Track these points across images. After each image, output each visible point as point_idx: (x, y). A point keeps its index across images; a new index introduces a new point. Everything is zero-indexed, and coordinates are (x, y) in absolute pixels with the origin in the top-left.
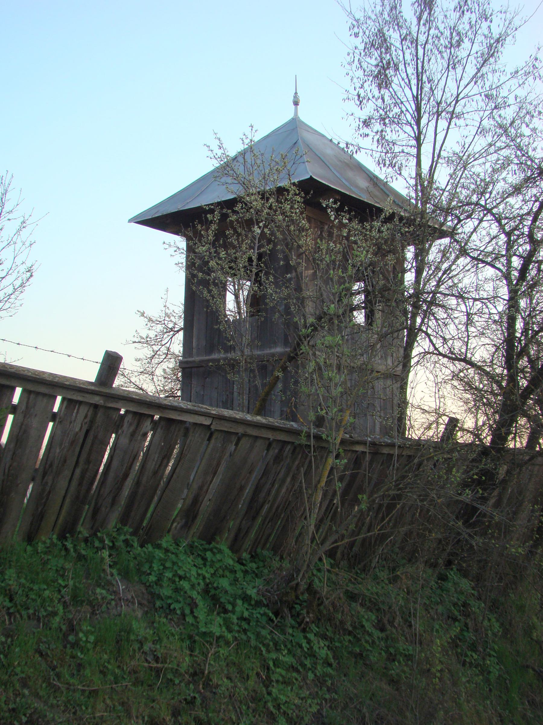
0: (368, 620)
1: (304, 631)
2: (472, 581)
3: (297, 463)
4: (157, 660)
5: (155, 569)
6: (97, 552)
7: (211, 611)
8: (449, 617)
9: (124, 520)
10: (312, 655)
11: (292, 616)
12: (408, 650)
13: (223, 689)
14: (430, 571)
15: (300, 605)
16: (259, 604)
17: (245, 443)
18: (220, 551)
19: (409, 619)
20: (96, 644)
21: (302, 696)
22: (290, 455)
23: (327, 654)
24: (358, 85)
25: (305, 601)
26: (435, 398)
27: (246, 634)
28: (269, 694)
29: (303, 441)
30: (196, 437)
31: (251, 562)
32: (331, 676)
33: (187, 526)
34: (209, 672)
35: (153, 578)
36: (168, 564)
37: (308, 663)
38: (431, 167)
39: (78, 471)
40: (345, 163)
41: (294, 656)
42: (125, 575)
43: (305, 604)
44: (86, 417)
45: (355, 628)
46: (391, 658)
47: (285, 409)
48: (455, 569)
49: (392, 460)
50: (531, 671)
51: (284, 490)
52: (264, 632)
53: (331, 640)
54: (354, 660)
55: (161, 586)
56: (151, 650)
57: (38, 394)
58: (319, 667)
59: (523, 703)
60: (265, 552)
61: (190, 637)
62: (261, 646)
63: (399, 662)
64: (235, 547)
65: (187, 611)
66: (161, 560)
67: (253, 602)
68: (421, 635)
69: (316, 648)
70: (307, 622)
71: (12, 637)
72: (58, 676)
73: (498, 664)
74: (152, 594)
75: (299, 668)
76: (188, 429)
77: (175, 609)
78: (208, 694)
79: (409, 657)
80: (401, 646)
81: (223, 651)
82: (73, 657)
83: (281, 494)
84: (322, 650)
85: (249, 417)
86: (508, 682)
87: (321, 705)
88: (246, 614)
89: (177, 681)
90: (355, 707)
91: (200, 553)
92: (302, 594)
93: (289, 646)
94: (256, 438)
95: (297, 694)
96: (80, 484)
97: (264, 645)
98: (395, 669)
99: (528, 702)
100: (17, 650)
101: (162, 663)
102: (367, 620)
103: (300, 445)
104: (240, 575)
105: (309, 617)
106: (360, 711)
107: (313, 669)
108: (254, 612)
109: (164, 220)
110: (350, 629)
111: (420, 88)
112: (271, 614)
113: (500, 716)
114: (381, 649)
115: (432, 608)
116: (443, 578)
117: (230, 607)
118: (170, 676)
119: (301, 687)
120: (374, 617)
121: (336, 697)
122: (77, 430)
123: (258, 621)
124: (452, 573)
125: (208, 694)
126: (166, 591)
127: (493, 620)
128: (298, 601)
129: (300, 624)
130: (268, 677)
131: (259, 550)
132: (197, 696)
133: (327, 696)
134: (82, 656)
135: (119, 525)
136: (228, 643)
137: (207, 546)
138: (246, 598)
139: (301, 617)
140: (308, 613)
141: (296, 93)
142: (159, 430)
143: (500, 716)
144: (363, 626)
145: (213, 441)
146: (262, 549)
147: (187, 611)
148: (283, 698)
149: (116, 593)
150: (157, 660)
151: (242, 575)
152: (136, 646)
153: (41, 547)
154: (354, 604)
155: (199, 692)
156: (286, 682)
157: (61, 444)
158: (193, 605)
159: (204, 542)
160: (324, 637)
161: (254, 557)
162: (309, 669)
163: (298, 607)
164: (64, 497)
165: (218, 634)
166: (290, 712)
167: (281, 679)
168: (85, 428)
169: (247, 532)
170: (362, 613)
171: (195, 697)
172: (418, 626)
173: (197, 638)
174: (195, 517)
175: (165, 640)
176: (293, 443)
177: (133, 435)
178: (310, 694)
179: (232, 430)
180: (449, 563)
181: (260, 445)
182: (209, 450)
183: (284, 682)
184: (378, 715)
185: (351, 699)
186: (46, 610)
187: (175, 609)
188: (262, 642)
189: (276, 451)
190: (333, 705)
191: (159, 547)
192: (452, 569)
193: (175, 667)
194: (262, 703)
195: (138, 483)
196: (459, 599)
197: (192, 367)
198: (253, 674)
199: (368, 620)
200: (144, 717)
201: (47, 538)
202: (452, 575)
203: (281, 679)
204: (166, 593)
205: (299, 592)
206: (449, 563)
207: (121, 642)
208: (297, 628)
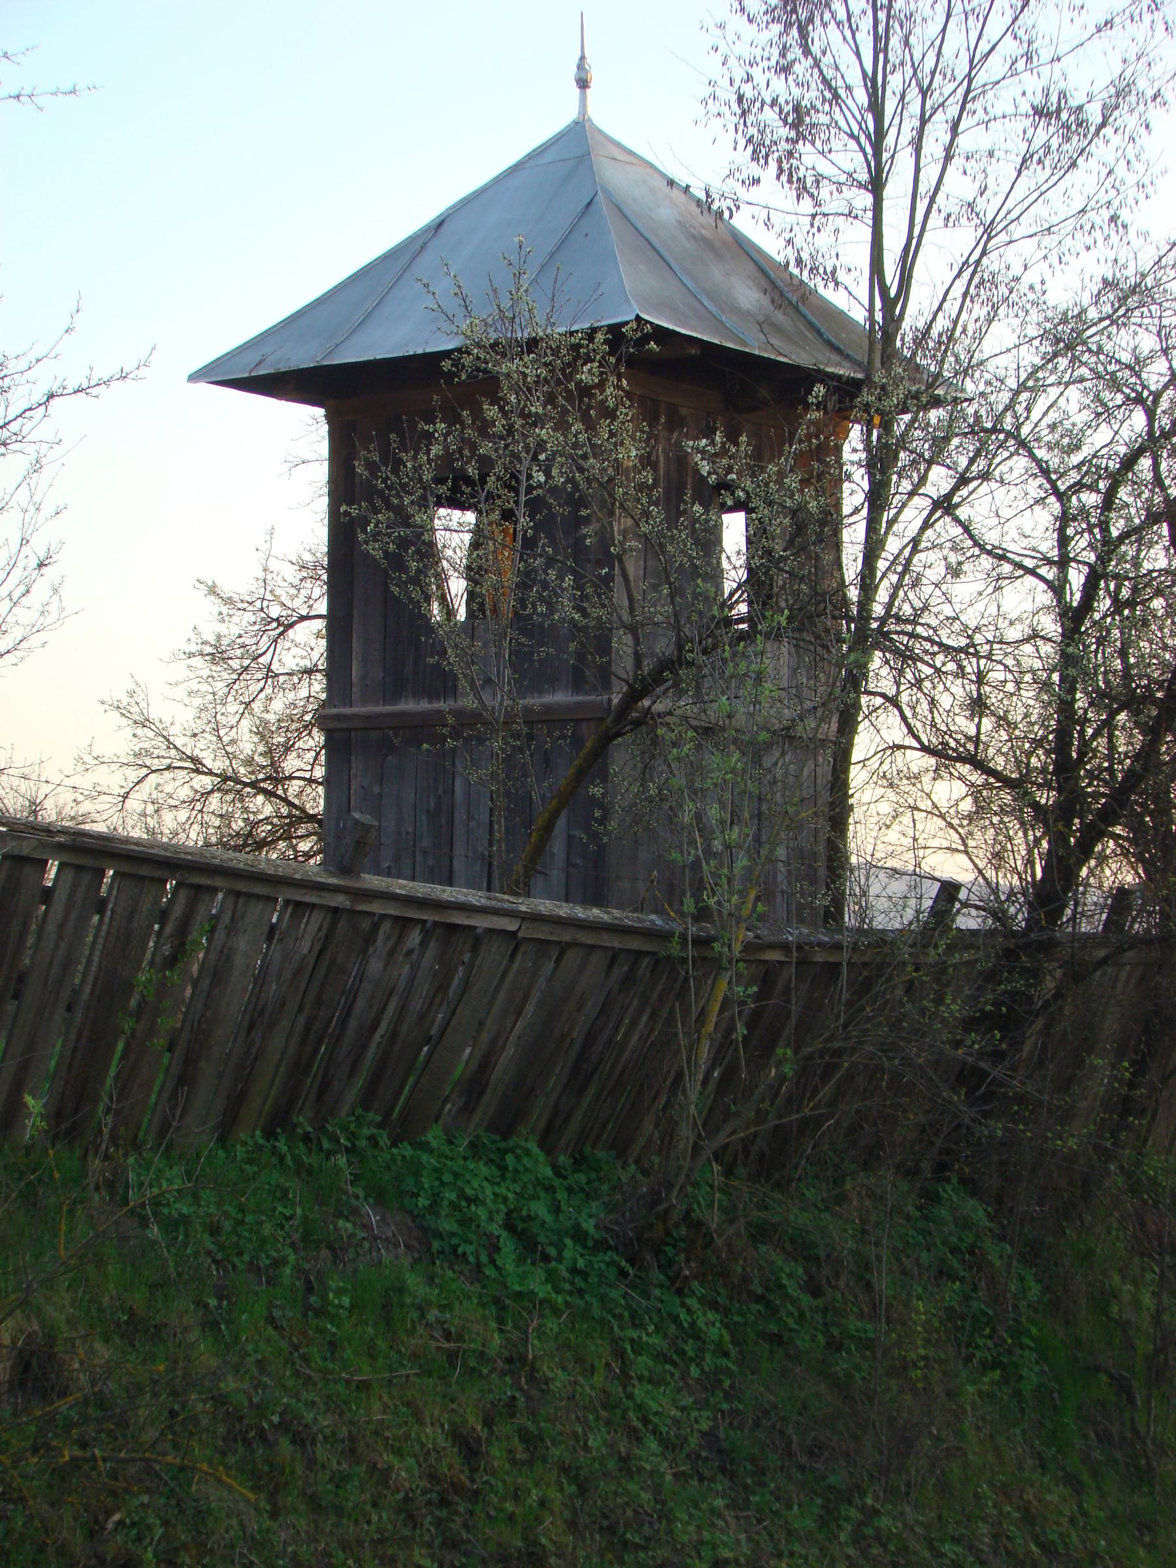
0: (791, 1275)
1: (680, 1292)
2: (988, 1204)
3: (660, 987)
4: (448, 1336)
5: (426, 1186)
6: (327, 1158)
7: (520, 1261)
8: (941, 1273)
9: (367, 1100)
10: (695, 1334)
11: (660, 1267)
12: (866, 1332)
13: (558, 1384)
14: (904, 1186)
15: (674, 1246)
16: (601, 1246)
17: (572, 958)
18: (528, 1153)
19: (867, 1276)
20: (351, 1310)
21: (683, 1403)
22: (648, 975)
23: (721, 1336)
24: (739, 74)
25: (682, 1240)
26: (916, 830)
27: (582, 1297)
28: (630, 1397)
29: (675, 949)
30: (492, 954)
31: (575, 1171)
32: (728, 1372)
33: (468, 1109)
34: (535, 1357)
35: (423, 1202)
36: (447, 1178)
37: (690, 1348)
38: (906, 249)
39: (302, 1020)
40: (704, 240)
41: (665, 1336)
42: (379, 1196)
43: (682, 1245)
44: (319, 930)
45: (767, 1289)
46: (835, 1346)
47: (577, 833)
48: (954, 1181)
49: (841, 976)
50: (1104, 1378)
51: (635, 1038)
52: (614, 1294)
53: (726, 1312)
54: (767, 1346)
55: (437, 1214)
56: (438, 1321)
57: (250, 896)
58: (708, 1357)
59: (1085, 1437)
60: (600, 1154)
61: (497, 1301)
62: (609, 1317)
63: (849, 1352)
64: (547, 1143)
65: (484, 1259)
66: (435, 1170)
67: (590, 1243)
68: (889, 1305)
69: (701, 1323)
70: (686, 1277)
71: (229, 1298)
72: (306, 1359)
73: (1037, 1363)
74: (424, 1229)
75: (675, 1357)
76: (476, 939)
77: (464, 1254)
78: (534, 1392)
79: (867, 1345)
80: (853, 1324)
81: (552, 1324)
82: (321, 1331)
83: (630, 1047)
84: (711, 1325)
85: (580, 912)
86: (1056, 1395)
87: (715, 1419)
88: (581, 1263)
89: (485, 1371)
90: (774, 1426)
91: (492, 1156)
92: (677, 1226)
93: (656, 1319)
94: (591, 948)
95: (674, 1401)
96: (303, 1042)
97: (614, 1316)
98: (841, 1366)
99: (1097, 1434)
100: (244, 1317)
101: (456, 1341)
102: (790, 1276)
103: (668, 958)
104: (561, 1195)
105: (690, 1268)
106: (781, 1432)
107: (699, 1360)
108: (594, 1259)
109: (264, 375)
110: (759, 1291)
111: (880, 45)
112: (623, 1263)
113: (1041, 1458)
114: (816, 1329)
115: (908, 1256)
116: (934, 1198)
117: (553, 1252)
118: (473, 1363)
119: (679, 1391)
120: (800, 1271)
121: (741, 1407)
122: (305, 951)
123: (601, 1275)
124: (949, 1188)
125: (534, 1392)
126: (448, 1225)
127: (1030, 1278)
128: (668, 1240)
129: (673, 1281)
130: (624, 1372)
131: (587, 1150)
132: (517, 1395)
133: (725, 1406)
134: (334, 1330)
135: (359, 1111)
136: (557, 1312)
137: (503, 1145)
138: (579, 1236)
139: (675, 1268)
140: (688, 1260)
141: (583, 58)
142: (432, 944)
143: (1041, 1458)
144: (782, 1287)
145: (519, 957)
146: (593, 1148)
147: (484, 1259)
148: (654, 1406)
149: (366, 1227)
150: (448, 1336)
151: (565, 1195)
152: (415, 1315)
153: (240, 1152)
154: (763, 1248)
155: (521, 1389)
156: (655, 1381)
157: (279, 977)
158: (494, 1248)
159: (497, 1137)
160: (714, 1306)
161: (579, 1162)
162: (691, 1360)
163: (669, 1250)
164: (278, 1066)
165: (541, 1295)
166: (664, 1429)
167: (646, 1373)
168: (317, 947)
169: (568, 1118)
170: (780, 1263)
171: (514, 1398)
172: (884, 1284)
173: (508, 1301)
174: (481, 1094)
175: (457, 1305)
176: (654, 954)
177: (391, 954)
178: (695, 1402)
179: (552, 938)
180: (941, 1169)
181: (598, 960)
182: (511, 975)
183: (650, 1381)
184: (814, 1439)
185: (766, 1413)
186: (268, 1257)
187: (464, 1254)
188: (609, 1311)
189: (626, 968)
190: (735, 1423)
191: (425, 1147)
192: (948, 1180)
193: (480, 1348)
194: (618, 1412)
195: (393, 1036)
196: (961, 1239)
197: (349, 730)
198: (600, 1365)
199: (791, 1275)
200: (442, 1426)
201: (249, 1136)
202: (949, 1191)
203: (646, 1373)
204: (447, 1227)
205: (670, 1224)
206: (941, 1169)
207: (388, 1306)
208: (669, 1288)
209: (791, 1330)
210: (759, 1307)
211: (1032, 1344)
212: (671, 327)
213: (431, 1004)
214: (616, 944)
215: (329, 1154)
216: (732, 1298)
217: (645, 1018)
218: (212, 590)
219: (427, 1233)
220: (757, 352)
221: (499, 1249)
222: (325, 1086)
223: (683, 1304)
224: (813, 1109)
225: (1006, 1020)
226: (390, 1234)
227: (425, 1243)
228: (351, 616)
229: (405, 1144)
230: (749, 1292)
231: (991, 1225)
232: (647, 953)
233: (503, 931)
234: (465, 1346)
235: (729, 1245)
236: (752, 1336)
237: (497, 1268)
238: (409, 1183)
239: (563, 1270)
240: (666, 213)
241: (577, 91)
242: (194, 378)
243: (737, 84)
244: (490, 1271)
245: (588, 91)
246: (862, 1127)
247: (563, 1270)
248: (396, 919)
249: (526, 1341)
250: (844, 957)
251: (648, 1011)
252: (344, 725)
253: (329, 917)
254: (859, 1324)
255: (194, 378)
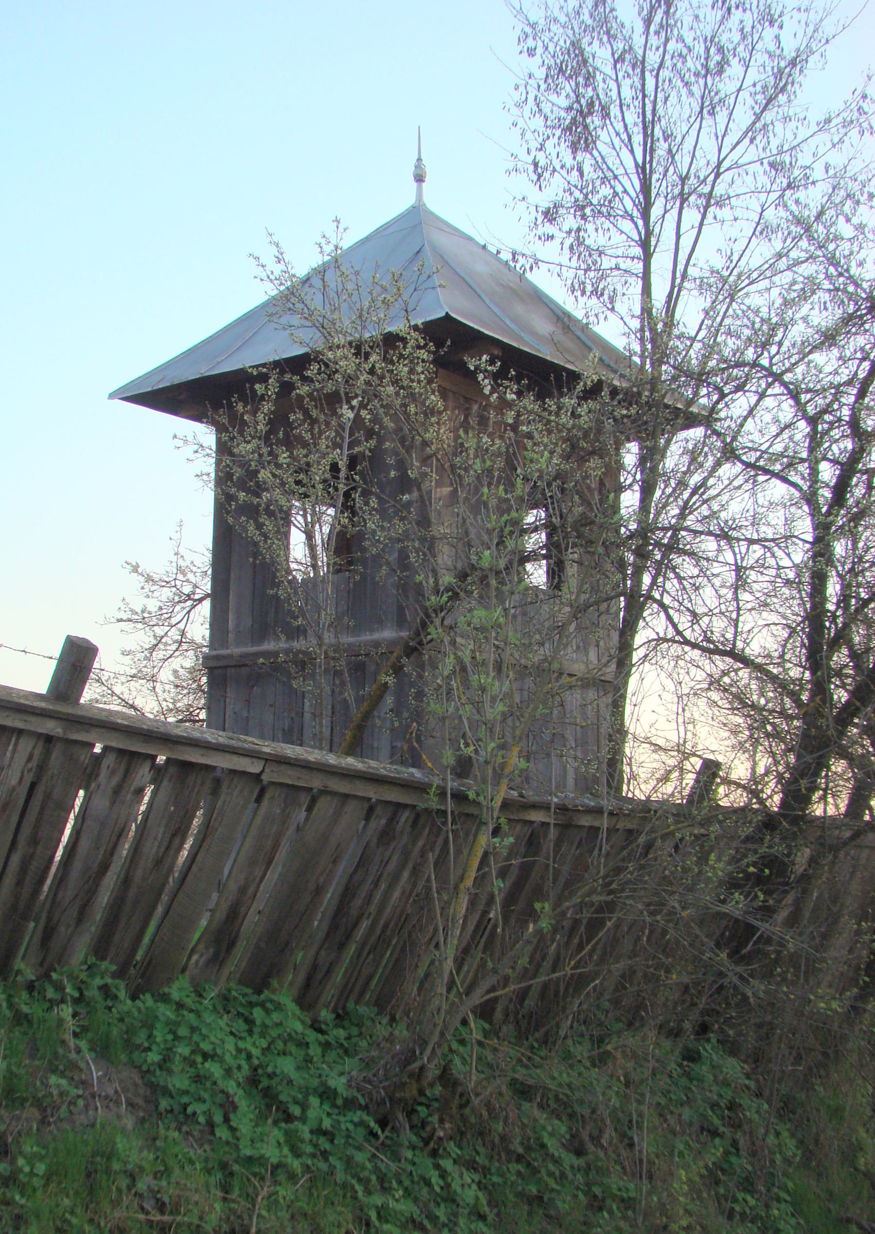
0: (553, 1132)
1: (434, 1154)
2: (745, 1062)
3: (420, 844)
4: (161, 1207)
5: (158, 1040)
8: (702, 1129)
9: (101, 949)
10: (449, 1198)
11: (412, 1127)
12: (628, 1190)
14: (667, 1044)
15: (428, 1106)
16: (350, 1104)
17: (324, 806)
18: (279, 1007)
22: (408, 829)
23: (477, 1198)
25: (436, 1100)
26: (678, 724)
27: (326, 1160)
29: (433, 803)
31: (336, 1026)
33: (217, 960)
35: (153, 1057)
36: (183, 1031)
41: (416, 1200)
42: (103, 1050)
43: (436, 1105)
44: (30, 759)
45: (528, 1148)
47: (399, 744)
48: (714, 1041)
51: (397, 894)
52: (360, 1157)
54: (526, 1207)
55: (170, 1072)
60: (362, 1009)
61: (224, 1166)
63: (611, 1212)
64: (306, 999)
65: (218, 1118)
66: (168, 1023)
67: (339, 1102)
68: (650, 1163)
69: (456, 1186)
70: (440, 1139)
73: (793, 1215)
74: (153, 1087)
76: (217, 781)
77: (194, 1114)
79: (628, 1204)
80: (615, 1182)
81: (285, 1192)
83: (392, 902)
85: (332, 759)
88: (327, 1124)
91: (241, 1010)
92: (431, 1085)
93: (407, 1183)
94: (346, 796)
96: (19, 883)
97: (360, 1180)
101: (171, 1213)
102: (552, 1135)
104: (315, 1051)
105: (444, 1129)
108: (342, 1119)
110: (520, 1150)
111: (649, 150)
112: (372, 1124)
114: (578, 1188)
117: (296, 1111)
120: (563, 1129)
122: (14, 782)
126: (179, 1081)
128: (423, 1099)
129: (426, 1142)
131: (351, 1005)
134: (23, 1201)
135: (92, 960)
136: (292, 1177)
137: (254, 998)
138: (327, 1094)
139: (428, 1129)
140: (441, 1121)
141: (419, 160)
142: (165, 782)
144: (543, 1146)
145: (265, 803)
146: (357, 1002)
147: (218, 1118)
150: (161, 1207)
151: (319, 1051)
152: (124, 1182)
154: (526, 1105)
158: (229, 1107)
159: (249, 991)
160: (472, 1166)
161: (341, 1017)
163: (422, 1110)
165: (274, 1160)
168: (28, 779)
170: (542, 1122)
173: (236, 1168)
174: (232, 944)
175: (177, 1171)
177: (117, 791)
180: (703, 1029)
181: (352, 810)
187: (194, 1114)
189: (383, 821)
191: (165, 998)
192: (708, 1040)
193: (196, 1221)
195: (126, 881)
197: (226, 667)
199: (553, 1132)
202: (709, 1050)
205: (425, 1083)
206: (703, 1029)
208: (422, 1150)
209: (553, 1190)
210: (521, 1167)
211: (788, 1199)
212: (476, 327)
213: (168, 848)
214: (374, 797)
215: (52, 1004)
216: (491, 1158)
217: (406, 874)
218: (135, 569)
219: (157, 1090)
220: (549, 358)
221: (235, 1108)
222: (48, 933)
223: (437, 1166)
224: (574, 968)
225: (770, 876)
226: (111, 1092)
227: (154, 1102)
228: (228, 579)
229: (148, 996)
230: (509, 1152)
231: (747, 1082)
232: (406, 806)
233: (244, 773)
234: (179, 1218)
235: (488, 1105)
236: (511, 1197)
237: (233, 1130)
238: (141, 1038)
239: (305, 1131)
240: (481, 268)
241: (415, 184)
242: (112, 396)
243: (533, 153)
244: (222, 1133)
245: (424, 184)
246: (625, 988)
247: (305, 1131)
248: (121, 752)
249: (250, 1211)
250: (605, 823)
251: (410, 866)
252: (220, 664)
253: (41, 744)
254: (621, 1183)
255: (112, 396)
